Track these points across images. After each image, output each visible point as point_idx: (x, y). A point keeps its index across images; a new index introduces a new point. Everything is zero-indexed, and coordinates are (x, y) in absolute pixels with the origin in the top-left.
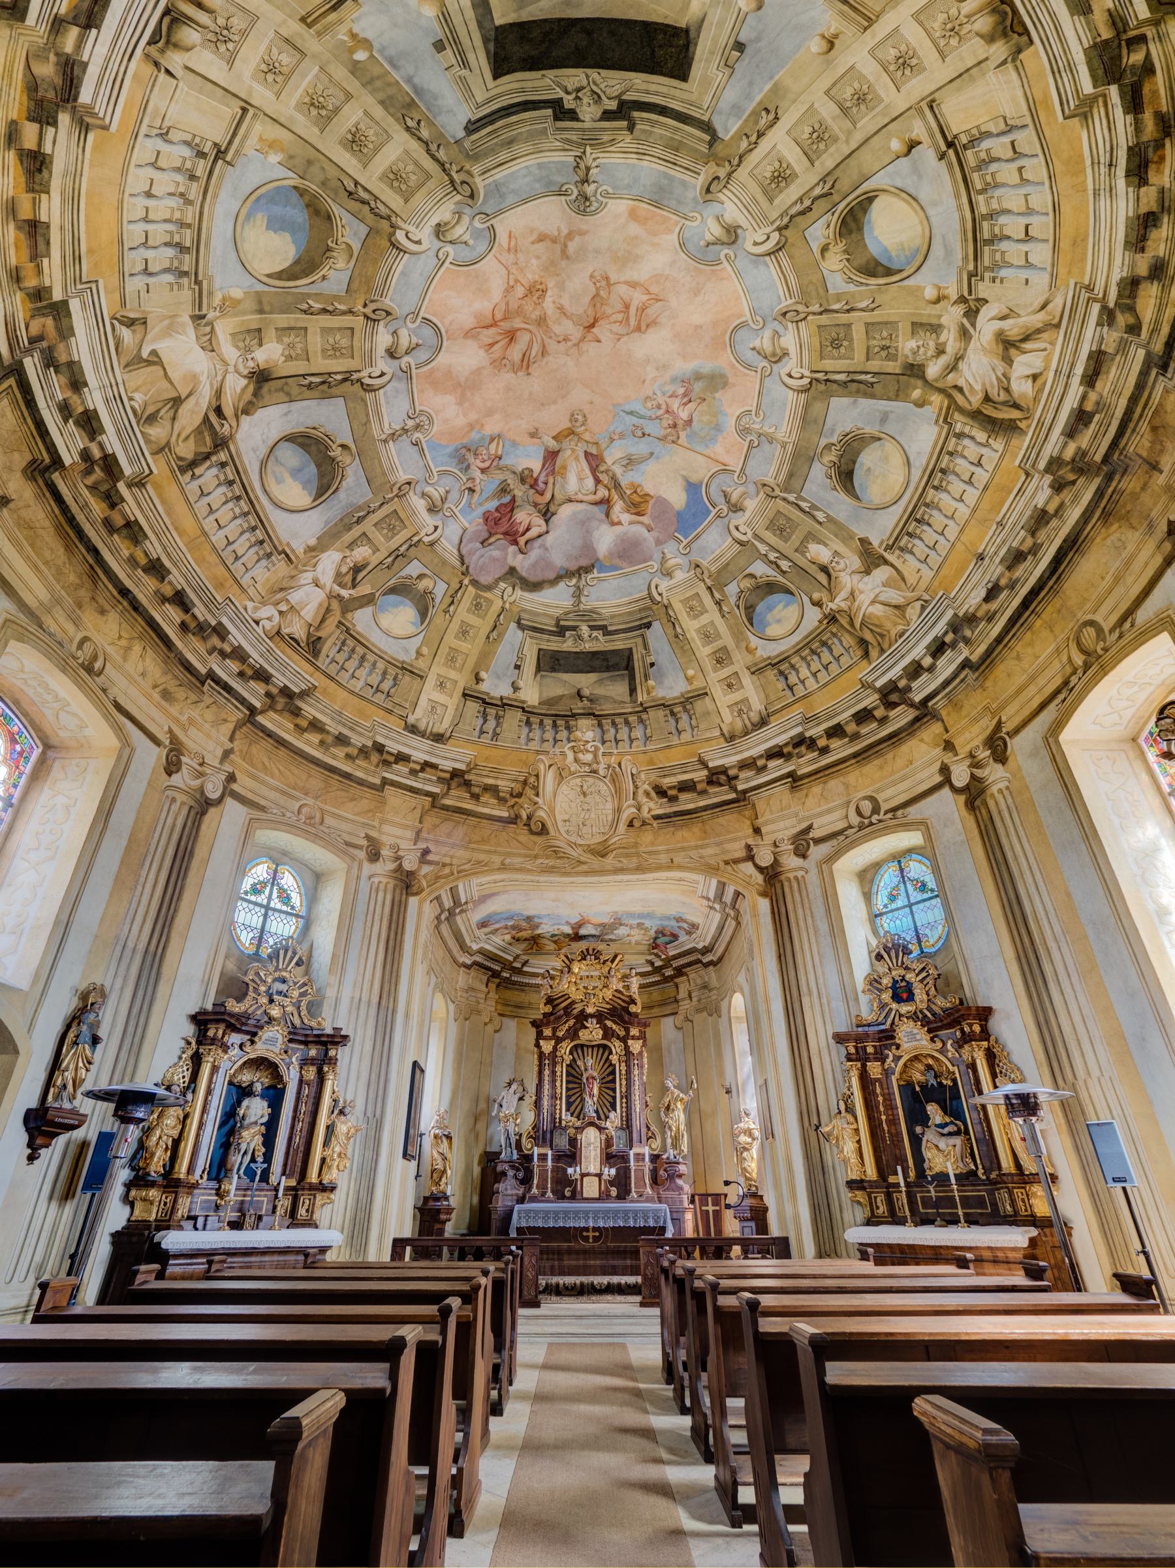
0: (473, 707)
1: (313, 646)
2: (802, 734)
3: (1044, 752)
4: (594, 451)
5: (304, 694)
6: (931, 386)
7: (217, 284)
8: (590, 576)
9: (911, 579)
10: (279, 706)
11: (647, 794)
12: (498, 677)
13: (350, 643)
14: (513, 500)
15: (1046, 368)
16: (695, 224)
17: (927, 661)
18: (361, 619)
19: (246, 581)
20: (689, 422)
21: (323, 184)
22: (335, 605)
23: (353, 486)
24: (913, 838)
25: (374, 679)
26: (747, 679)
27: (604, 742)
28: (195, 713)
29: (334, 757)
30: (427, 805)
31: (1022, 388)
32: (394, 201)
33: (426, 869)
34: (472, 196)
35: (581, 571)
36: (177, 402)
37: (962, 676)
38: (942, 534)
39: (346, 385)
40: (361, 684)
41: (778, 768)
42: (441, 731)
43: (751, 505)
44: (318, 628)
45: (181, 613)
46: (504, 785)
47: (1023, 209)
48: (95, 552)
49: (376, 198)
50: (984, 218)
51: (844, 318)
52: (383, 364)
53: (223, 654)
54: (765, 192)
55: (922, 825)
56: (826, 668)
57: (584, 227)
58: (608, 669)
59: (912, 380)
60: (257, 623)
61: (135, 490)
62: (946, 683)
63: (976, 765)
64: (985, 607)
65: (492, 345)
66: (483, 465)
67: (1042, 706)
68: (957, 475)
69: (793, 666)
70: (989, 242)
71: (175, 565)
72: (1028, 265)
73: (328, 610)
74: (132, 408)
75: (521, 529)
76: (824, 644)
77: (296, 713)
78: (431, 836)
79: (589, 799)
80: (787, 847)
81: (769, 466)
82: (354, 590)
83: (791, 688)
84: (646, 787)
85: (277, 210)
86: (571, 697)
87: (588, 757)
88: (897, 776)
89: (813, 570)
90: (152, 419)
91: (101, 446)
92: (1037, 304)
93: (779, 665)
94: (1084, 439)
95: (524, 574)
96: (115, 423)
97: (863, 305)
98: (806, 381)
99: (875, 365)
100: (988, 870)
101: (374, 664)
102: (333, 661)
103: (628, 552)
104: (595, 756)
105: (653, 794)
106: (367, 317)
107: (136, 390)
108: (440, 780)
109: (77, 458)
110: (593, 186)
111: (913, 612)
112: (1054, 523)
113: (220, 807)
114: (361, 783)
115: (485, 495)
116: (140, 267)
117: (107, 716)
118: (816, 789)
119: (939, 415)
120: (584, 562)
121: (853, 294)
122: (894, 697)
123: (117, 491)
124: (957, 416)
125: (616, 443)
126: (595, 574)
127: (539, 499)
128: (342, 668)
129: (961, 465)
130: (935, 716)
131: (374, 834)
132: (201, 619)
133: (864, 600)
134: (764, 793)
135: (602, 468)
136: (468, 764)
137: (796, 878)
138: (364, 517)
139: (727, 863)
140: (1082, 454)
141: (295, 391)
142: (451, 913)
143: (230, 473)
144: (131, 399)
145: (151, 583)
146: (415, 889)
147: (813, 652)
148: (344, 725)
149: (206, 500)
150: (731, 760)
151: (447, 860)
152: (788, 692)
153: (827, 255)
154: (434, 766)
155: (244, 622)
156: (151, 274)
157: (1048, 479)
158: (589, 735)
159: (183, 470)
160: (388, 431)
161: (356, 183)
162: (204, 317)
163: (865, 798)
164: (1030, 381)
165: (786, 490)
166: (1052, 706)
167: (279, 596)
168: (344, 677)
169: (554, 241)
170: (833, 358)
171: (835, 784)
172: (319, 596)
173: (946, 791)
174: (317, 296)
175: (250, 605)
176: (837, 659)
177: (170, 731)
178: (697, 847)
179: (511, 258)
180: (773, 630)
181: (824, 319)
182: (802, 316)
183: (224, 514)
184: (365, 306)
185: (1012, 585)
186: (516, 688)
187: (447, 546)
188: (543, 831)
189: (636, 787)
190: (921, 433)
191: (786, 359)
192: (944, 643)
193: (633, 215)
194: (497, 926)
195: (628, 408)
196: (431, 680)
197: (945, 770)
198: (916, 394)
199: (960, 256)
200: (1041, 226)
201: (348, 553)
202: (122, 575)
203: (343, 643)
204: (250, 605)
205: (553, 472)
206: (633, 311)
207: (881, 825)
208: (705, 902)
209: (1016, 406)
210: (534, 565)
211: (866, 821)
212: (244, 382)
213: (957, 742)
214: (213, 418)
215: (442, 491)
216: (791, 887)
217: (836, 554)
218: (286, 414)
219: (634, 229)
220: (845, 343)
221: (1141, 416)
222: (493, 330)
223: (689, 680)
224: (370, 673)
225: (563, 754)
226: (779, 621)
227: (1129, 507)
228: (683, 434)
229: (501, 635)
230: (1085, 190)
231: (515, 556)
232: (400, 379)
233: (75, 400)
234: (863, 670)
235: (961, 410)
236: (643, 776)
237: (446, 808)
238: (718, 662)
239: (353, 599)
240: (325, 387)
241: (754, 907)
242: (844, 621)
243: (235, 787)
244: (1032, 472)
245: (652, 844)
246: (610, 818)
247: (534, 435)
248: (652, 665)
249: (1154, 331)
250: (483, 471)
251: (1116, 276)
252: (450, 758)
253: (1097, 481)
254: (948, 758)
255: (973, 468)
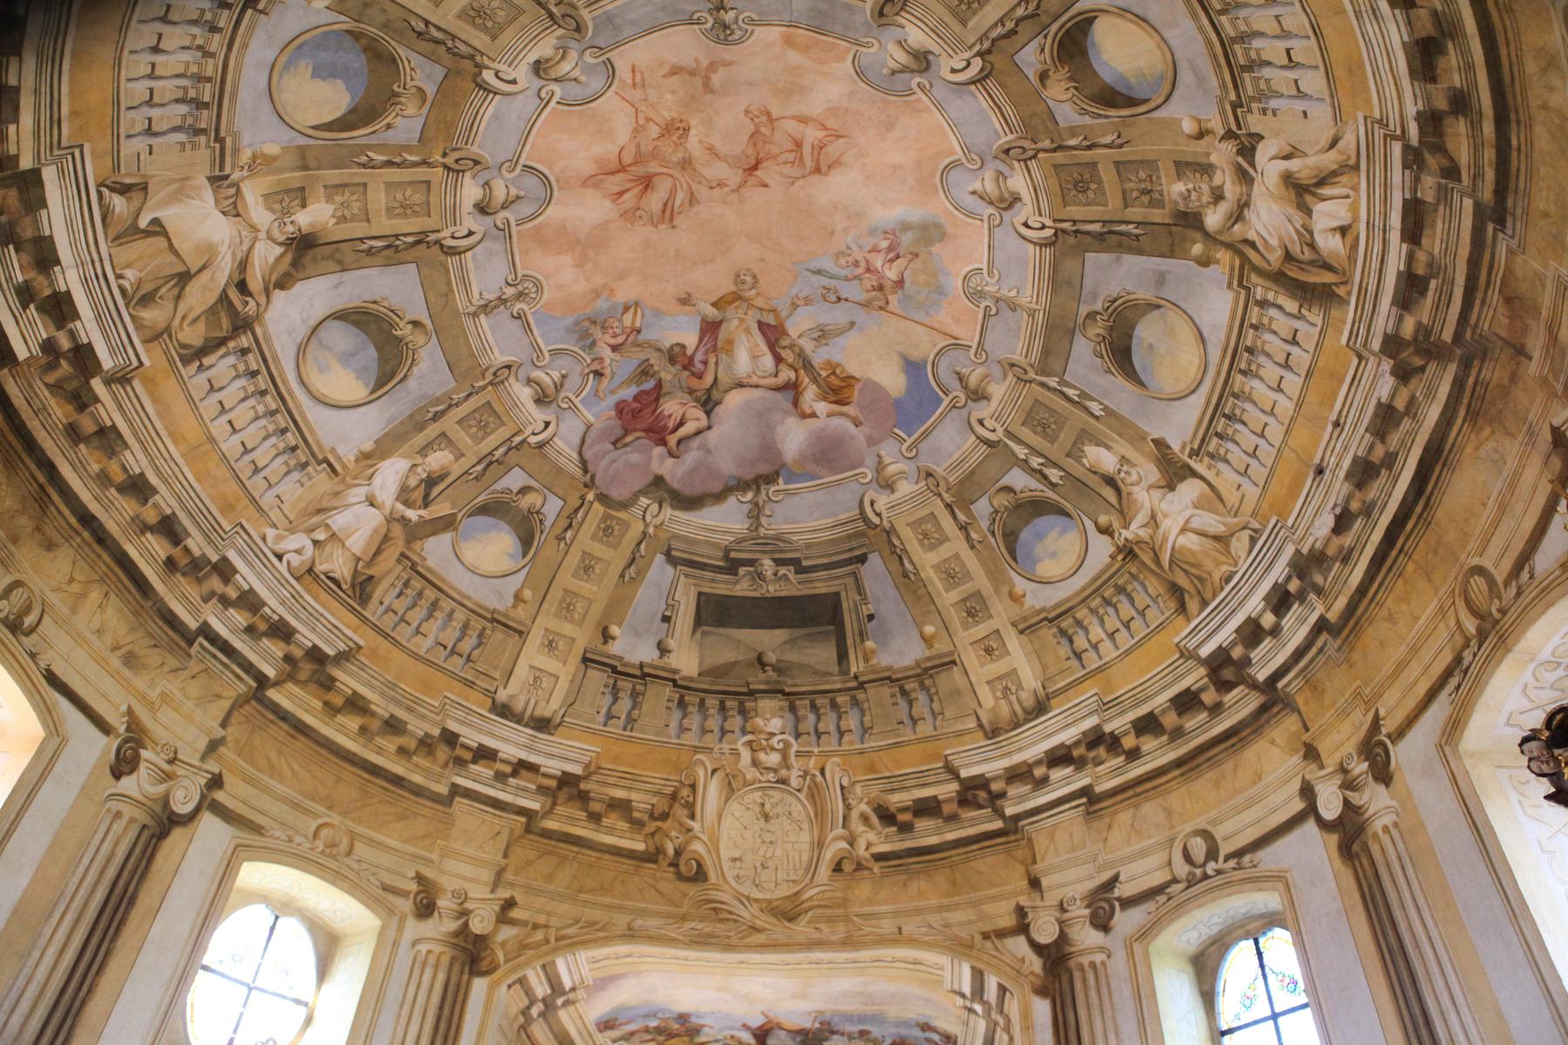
0: (597, 678)
1: (361, 589)
2: (1098, 728)
3: (1440, 769)
4: (771, 320)
5: (343, 657)
6: (1215, 239)
7: (246, 140)
8: (773, 489)
9: (1232, 498)
10: (303, 676)
11: (865, 819)
12: (637, 633)
13: (417, 583)
14: (659, 384)
15: (1356, 219)
16: (872, 50)
17: (1268, 620)
18: (435, 550)
19: (267, 500)
20: (900, 283)
21: (385, 26)
22: (397, 530)
23: (429, 372)
24: (1268, 900)
25: (449, 637)
26: (1013, 642)
27: (798, 736)
28: (172, 686)
29: (380, 751)
30: (519, 830)
31: (1331, 244)
32: (479, 40)
33: (506, 933)
34: (578, 29)
35: (761, 478)
36: (184, 278)
37: (1319, 643)
38: (1262, 435)
39: (426, 250)
40: (427, 643)
41: (1065, 781)
42: (547, 713)
43: (997, 390)
44: (369, 564)
45: (168, 545)
46: (641, 800)
47: (1278, 31)
48: (50, 468)
49: (454, 37)
50: (1234, 40)
51: (1086, 156)
52: (470, 221)
53: (225, 602)
54: (955, 14)
55: (1279, 879)
56: (1127, 626)
57: (728, 57)
58: (803, 623)
59: (1190, 233)
60: (280, 557)
61: (116, 387)
62: (1299, 654)
63: (1349, 785)
64: (1336, 541)
65: (621, 194)
66: (613, 341)
67: (1431, 695)
68: (1268, 355)
69: (1079, 623)
70: (1249, 68)
71: (165, 482)
72: (1301, 95)
73: (386, 538)
74: (123, 290)
75: (671, 424)
76: (1121, 590)
77: (328, 684)
78: (520, 880)
79: (772, 826)
80: (1080, 911)
81: (1016, 341)
82: (426, 511)
83: (1078, 656)
84: (864, 807)
85: (325, 56)
86: (749, 664)
87: (774, 759)
88: (1239, 799)
89: (1094, 482)
90: (147, 299)
91: (73, 335)
92: (1325, 140)
93: (1060, 621)
94: (1424, 311)
95: (676, 485)
96: (94, 306)
97: (1108, 140)
98: (1048, 233)
99: (1136, 213)
100: (1378, 963)
101: (451, 615)
102: (390, 609)
103: (828, 456)
104: (785, 757)
105: (875, 820)
106: (447, 167)
107: (128, 266)
108: (542, 790)
109: (36, 350)
110: (732, 14)
111: (1240, 544)
112: (1406, 424)
113: (191, 827)
114: (418, 791)
115: (618, 380)
116: (141, 126)
117: (31, 692)
118: (1125, 817)
119: (1231, 277)
120: (763, 469)
121: (1091, 127)
122: (1227, 673)
123: (91, 389)
124: (1254, 278)
125: (801, 311)
126: (781, 485)
127: (695, 383)
128: (402, 620)
129: (1273, 344)
130: (1289, 705)
131: (428, 873)
132: (197, 552)
133: (1171, 526)
134: (1046, 821)
135: (785, 342)
136: (587, 766)
137: (1093, 965)
138: (444, 412)
139: (985, 936)
140: (1423, 331)
141: (349, 257)
142: (549, 1007)
143: (253, 362)
144: (119, 277)
145: (127, 506)
146: (484, 965)
147: (1107, 602)
148: (399, 704)
149: (217, 396)
150: (993, 767)
151: (541, 919)
152: (1074, 662)
153: (1048, 83)
154: (533, 768)
155: (261, 556)
156: (156, 134)
157: (1387, 365)
158: (775, 724)
159: (186, 361)
160: (477, 301)
161: (427, 23)
162: (227, 177)
163: (1197, 833)
164: (1338, 237)
165: (1043, 371)
166: (1443, 696)
167: (316, 520)
168: (403, 634)
169: (692, 73)
170: (1080, 204)
171: (1150, 810)
172: (374, 518)
173: (1310, 826)
174: (378, 148)
175: (271, 533)
176: (1142, 613)
177: (130, 712)
178: (941, 908)
179: (638, 93)
180: (1046, 569)
181: (1059, 157)
182: (1030, 153)
183: (242, 414)
184: (445, 155)
185: (1368, 510)
186: (663, 650)
187: (565, 448)
188: (700, 875)
189: (848, 808)
190: (1214, 302)
191: (1018, 205)
192: (1287, 593)
193: (788, 41)
194: (631, 1027)
195: (814, 266)
196: (536, 637)
197: (1307, 791)
198: (1197, 249)
199: (1215, 84)
200: (1304, 49)
201: (419, 460)
202: (85, 497)
203: (406, 584)
204: (271, 533)
205: (715, 348)
206: (807, 149)
207: (1219, 880)
208: (959, 1001)
209: (1327, 267)
210: (692, 472)
211: (1198, 872)
212: (279, 250)
213: (1323, 747)
214: (234, 295)
215: (556, 375)
216: (1084, 981)
217: (1124, 460)
218: (336, 287)
219: (794, 57)
220: (1093, 186)
221: (1488, 283)
222: (621, 176)
223: (928, 641)
224: (444, 627)
225: (735, 753)
226: (1053, 555)
227: (1499, 405)
228: (893, 299)
229: (641, 573)
230: (1344, 12)
231: (662, 461)
232: (495, 238)
233: (40, 282)
234: (1181, 632)
235: (1260, 272)
236: (858, 789)
237: (547, 834)
238: (970, 614)
239: (423, 523)
240: (390, 252)
241: (1026, 1014)
242: (1146, 558)
243: (220, 796)
244: (1365, 353)
245: (870, 901)
246: (806, 856)
247: (685, 301)
248: (871, 617)
249: (1477, 176)
250: (614, 348)
251: (1411, 110)
252: (559, 755)
253: (1452, 368)
254: (1312, 772)
255: (1288, 348)
